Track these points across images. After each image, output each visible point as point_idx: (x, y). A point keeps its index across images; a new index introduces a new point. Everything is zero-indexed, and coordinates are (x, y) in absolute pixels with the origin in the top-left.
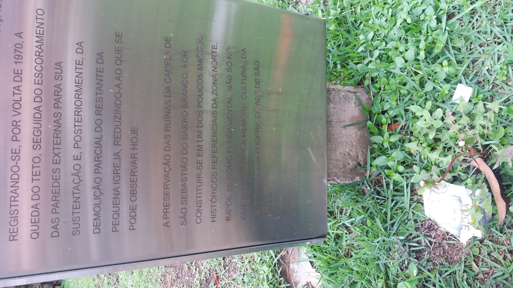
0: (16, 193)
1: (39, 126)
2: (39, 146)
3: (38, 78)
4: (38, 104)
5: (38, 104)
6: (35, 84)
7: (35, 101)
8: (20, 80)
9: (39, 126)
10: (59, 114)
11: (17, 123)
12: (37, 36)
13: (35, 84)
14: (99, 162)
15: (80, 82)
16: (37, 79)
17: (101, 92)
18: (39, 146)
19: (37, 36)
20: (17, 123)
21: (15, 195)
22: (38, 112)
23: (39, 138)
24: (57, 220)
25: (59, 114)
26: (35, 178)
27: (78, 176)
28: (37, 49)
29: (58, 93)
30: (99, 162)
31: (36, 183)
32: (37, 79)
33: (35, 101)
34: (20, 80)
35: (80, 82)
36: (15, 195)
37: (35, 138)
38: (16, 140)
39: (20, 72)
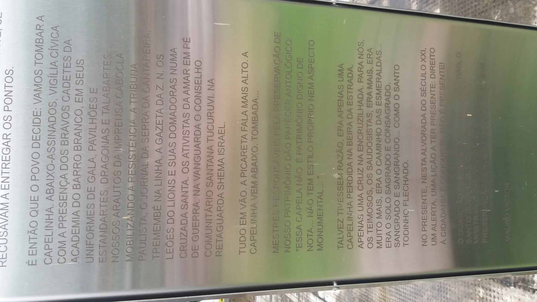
1: (36, 206)
3: (103, 196)
4: (76, 209)
5: (76, 209)
7: (73, 206)
8: (66, 168)
9: (36, 206)
11: (40, 27)
14: (41, 31)
16: (102, 197)
17: (187, 125)
20: (40, 27)
23: (8, 156)
30: (41, 31)
32: (102, 197)
33: (73, 206)
34: (66, 168)
37: (4, 156)
38: (8, 111)
39: (301, 60)
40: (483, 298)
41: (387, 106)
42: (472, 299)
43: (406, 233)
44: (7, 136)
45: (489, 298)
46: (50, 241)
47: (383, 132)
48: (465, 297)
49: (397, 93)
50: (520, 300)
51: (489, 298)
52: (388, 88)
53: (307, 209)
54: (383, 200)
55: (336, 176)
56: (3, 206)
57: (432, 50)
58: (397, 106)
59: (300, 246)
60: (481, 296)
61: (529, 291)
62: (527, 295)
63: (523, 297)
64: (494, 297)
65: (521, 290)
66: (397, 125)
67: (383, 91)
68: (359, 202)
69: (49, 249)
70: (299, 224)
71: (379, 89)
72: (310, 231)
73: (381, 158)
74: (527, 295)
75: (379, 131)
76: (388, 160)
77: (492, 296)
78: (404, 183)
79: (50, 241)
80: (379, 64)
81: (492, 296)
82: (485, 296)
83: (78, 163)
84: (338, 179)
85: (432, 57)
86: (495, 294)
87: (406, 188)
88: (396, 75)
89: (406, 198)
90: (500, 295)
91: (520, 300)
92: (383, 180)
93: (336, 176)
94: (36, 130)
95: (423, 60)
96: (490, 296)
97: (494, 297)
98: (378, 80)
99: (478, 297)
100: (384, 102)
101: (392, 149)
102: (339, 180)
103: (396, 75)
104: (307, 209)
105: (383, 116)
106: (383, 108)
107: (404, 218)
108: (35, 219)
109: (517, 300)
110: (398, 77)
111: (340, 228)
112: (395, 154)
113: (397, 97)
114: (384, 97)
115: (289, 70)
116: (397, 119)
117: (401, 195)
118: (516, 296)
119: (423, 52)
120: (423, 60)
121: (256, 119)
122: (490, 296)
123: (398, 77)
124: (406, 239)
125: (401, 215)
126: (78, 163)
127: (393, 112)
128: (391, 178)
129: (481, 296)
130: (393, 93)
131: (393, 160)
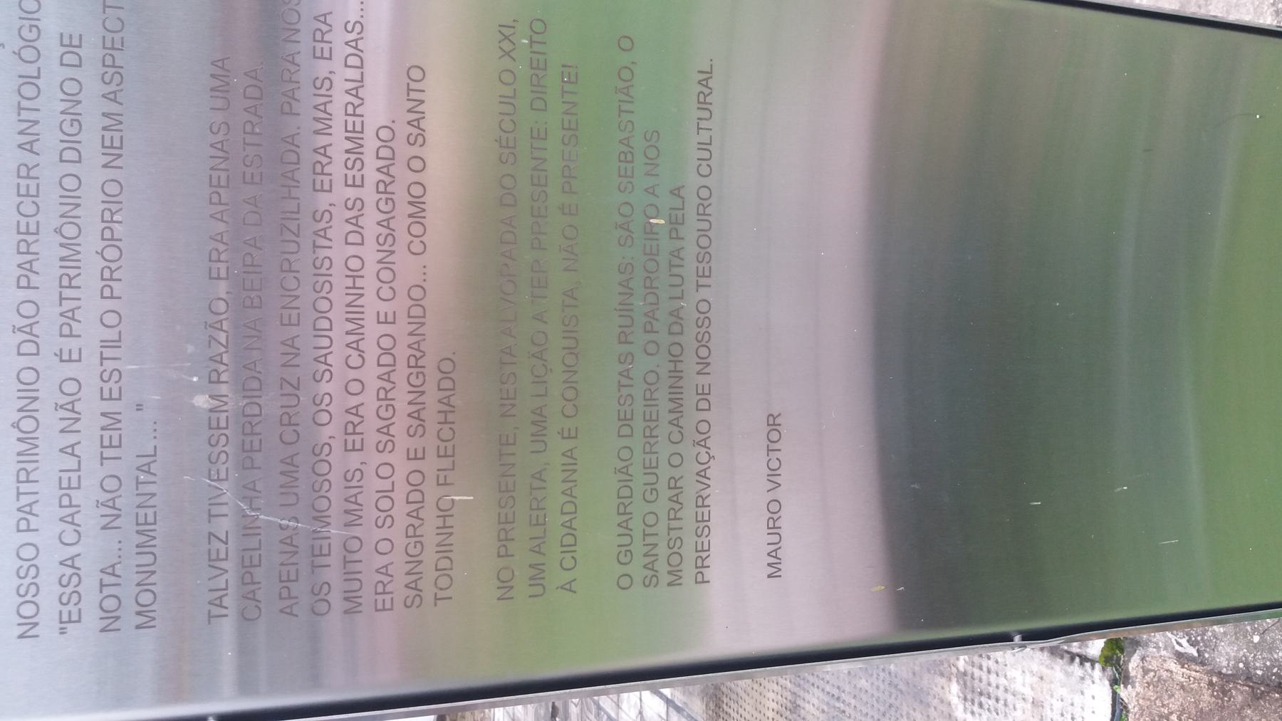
0: (357, 415)
2: (358, 162)
3: (354, 172)
6: (102, 399)
10: (359, 203)
12: (347, 138)
13: (379, 322)
15: (358, 128)
18: (358, 162)
19: (347, 138)
21: (356, 420)
22: (355, 228)
24: (359, 203)
25: (359, 203)
26: (109, 453)
27: (357, 349)
28: (350, 99)
29: (355, 426)
31: (110, 467)
35: (358, 128)
36: (356, 420)
39: (75, 42)
40: (965, 674)
41: (384, 189)
42: (942, 675)
43: (444, 564)
44: (29, 170)
45: (977, 672)
46: (74, 484)
47: (371, 267)
48: (929, 671)
49: (415, 151)
50: (1042, 678)
51: (977, 672)
52: (384, 134)
53: (99, 504)
54: (370, 471)
55: (202, 401)
56: (353, 326)
57: (538, 27)
58: (417, 190)
59: (75, 617)
60: (962, 669)
61: (1062, 658)
62: (1057, 668)
63: (1049, 672)
64: (989, 671)
65: (1046, 654)
66: (417, 247)
67: (371, 144)
68: (284, 479)
69: (71, 506)
70: (73, 550)
71: (355, 136)
72: (110, 570)
73: (362, 345)
74: (1057, 668)
75: (355, 264)
76: (387, 351)
77: (985, 669)
78: (441, 418)
79: (74, 484)
80: (353, 61)
81: (985, 669)
82: (969, 668)
83: (114, 266)
84: (211, 410)
85: (536, 47)
86: (991, 663)
87: (446, 434)
88: (413, 95)
89: (446, 463)
90: (1001, 666)
91: (1042, 678)
92: (369, 411)
93: (202, 401)
94: (508, 125)
95: (508, 54)
96: (981, 668)
97: (989, 671)
98: (354, 111)
99: (954, 670)
100: (372, 176)
101: (402, 320)
102: (214, 416)
103: (413, 95)
104: (99, 504)
105: (370, 220)
106: (369, 194)
107: (440, 522)
108: (353, 374)
109: (1036, 679)
110: (422, 102)
111: (218, 559)
112: (411, 334)
113: (416, 164)
114: (371, 164)
115: (31, 70)
116: (416, 229)
117: (431, 453)
118: (1035, 668)
119: (507, 31)
120: (508, 54)
121: (629, 157)
122: (981, 668)
123: (422, 102)
124: (443, 582)
125: (429, 513)
126: (114, 266)
127: (404, 209)
128: (397, 404)
129: (962, 669)
130: (403, 151)
131: (402, 352)
